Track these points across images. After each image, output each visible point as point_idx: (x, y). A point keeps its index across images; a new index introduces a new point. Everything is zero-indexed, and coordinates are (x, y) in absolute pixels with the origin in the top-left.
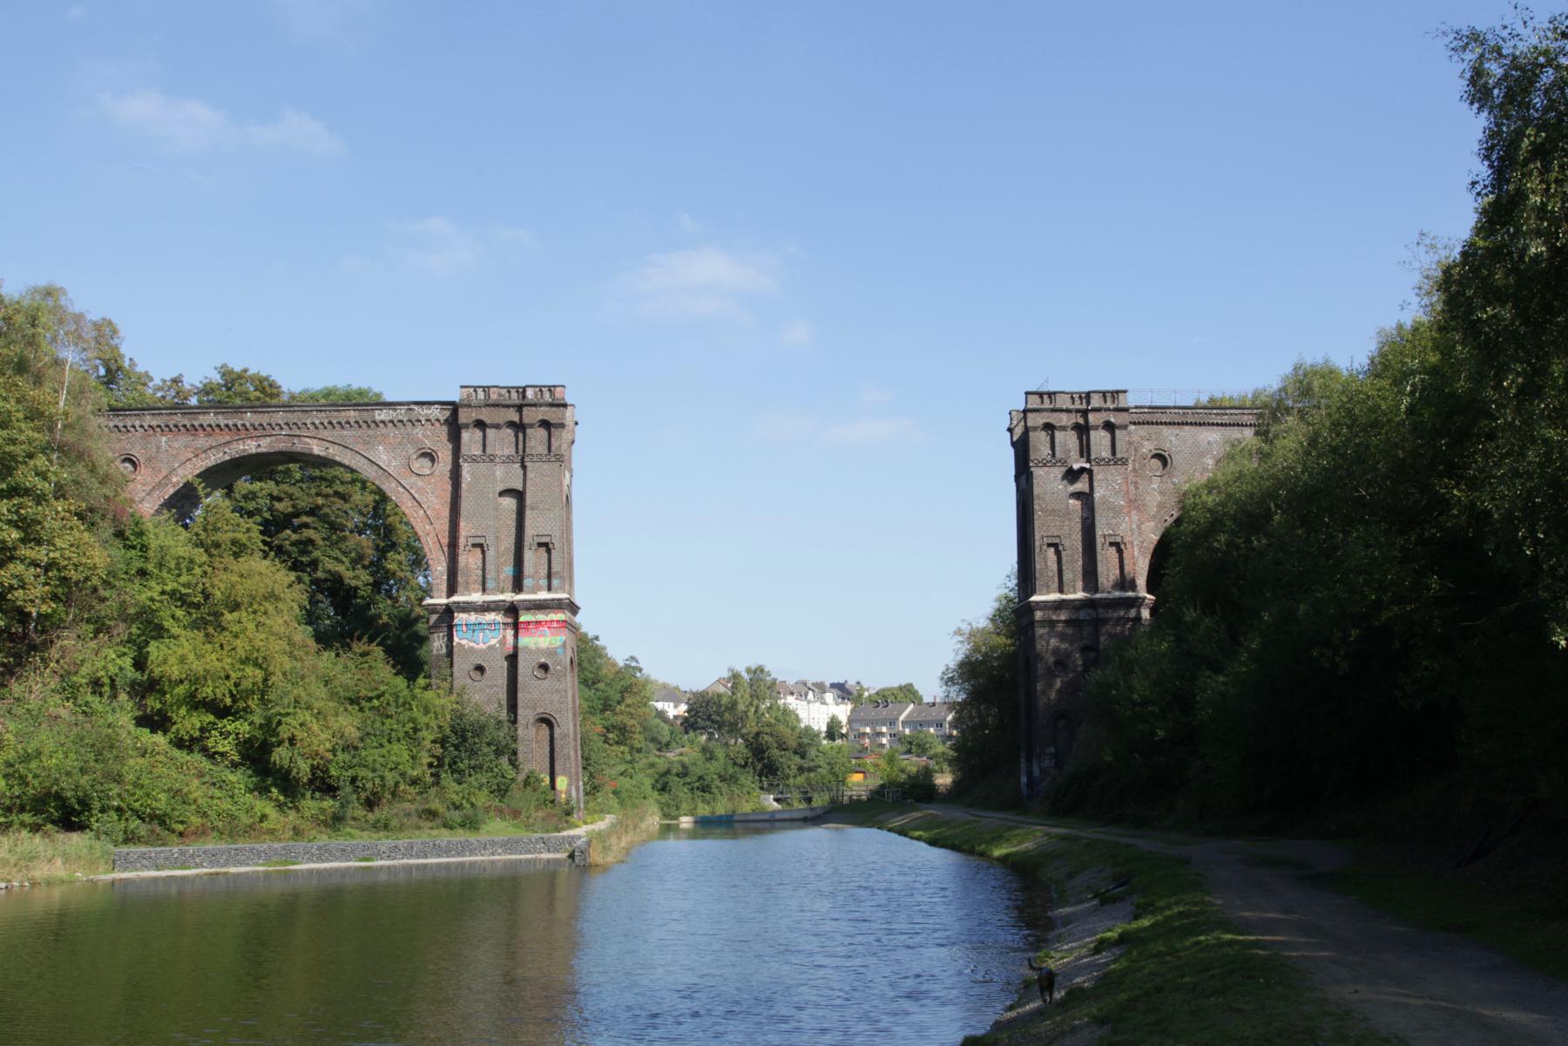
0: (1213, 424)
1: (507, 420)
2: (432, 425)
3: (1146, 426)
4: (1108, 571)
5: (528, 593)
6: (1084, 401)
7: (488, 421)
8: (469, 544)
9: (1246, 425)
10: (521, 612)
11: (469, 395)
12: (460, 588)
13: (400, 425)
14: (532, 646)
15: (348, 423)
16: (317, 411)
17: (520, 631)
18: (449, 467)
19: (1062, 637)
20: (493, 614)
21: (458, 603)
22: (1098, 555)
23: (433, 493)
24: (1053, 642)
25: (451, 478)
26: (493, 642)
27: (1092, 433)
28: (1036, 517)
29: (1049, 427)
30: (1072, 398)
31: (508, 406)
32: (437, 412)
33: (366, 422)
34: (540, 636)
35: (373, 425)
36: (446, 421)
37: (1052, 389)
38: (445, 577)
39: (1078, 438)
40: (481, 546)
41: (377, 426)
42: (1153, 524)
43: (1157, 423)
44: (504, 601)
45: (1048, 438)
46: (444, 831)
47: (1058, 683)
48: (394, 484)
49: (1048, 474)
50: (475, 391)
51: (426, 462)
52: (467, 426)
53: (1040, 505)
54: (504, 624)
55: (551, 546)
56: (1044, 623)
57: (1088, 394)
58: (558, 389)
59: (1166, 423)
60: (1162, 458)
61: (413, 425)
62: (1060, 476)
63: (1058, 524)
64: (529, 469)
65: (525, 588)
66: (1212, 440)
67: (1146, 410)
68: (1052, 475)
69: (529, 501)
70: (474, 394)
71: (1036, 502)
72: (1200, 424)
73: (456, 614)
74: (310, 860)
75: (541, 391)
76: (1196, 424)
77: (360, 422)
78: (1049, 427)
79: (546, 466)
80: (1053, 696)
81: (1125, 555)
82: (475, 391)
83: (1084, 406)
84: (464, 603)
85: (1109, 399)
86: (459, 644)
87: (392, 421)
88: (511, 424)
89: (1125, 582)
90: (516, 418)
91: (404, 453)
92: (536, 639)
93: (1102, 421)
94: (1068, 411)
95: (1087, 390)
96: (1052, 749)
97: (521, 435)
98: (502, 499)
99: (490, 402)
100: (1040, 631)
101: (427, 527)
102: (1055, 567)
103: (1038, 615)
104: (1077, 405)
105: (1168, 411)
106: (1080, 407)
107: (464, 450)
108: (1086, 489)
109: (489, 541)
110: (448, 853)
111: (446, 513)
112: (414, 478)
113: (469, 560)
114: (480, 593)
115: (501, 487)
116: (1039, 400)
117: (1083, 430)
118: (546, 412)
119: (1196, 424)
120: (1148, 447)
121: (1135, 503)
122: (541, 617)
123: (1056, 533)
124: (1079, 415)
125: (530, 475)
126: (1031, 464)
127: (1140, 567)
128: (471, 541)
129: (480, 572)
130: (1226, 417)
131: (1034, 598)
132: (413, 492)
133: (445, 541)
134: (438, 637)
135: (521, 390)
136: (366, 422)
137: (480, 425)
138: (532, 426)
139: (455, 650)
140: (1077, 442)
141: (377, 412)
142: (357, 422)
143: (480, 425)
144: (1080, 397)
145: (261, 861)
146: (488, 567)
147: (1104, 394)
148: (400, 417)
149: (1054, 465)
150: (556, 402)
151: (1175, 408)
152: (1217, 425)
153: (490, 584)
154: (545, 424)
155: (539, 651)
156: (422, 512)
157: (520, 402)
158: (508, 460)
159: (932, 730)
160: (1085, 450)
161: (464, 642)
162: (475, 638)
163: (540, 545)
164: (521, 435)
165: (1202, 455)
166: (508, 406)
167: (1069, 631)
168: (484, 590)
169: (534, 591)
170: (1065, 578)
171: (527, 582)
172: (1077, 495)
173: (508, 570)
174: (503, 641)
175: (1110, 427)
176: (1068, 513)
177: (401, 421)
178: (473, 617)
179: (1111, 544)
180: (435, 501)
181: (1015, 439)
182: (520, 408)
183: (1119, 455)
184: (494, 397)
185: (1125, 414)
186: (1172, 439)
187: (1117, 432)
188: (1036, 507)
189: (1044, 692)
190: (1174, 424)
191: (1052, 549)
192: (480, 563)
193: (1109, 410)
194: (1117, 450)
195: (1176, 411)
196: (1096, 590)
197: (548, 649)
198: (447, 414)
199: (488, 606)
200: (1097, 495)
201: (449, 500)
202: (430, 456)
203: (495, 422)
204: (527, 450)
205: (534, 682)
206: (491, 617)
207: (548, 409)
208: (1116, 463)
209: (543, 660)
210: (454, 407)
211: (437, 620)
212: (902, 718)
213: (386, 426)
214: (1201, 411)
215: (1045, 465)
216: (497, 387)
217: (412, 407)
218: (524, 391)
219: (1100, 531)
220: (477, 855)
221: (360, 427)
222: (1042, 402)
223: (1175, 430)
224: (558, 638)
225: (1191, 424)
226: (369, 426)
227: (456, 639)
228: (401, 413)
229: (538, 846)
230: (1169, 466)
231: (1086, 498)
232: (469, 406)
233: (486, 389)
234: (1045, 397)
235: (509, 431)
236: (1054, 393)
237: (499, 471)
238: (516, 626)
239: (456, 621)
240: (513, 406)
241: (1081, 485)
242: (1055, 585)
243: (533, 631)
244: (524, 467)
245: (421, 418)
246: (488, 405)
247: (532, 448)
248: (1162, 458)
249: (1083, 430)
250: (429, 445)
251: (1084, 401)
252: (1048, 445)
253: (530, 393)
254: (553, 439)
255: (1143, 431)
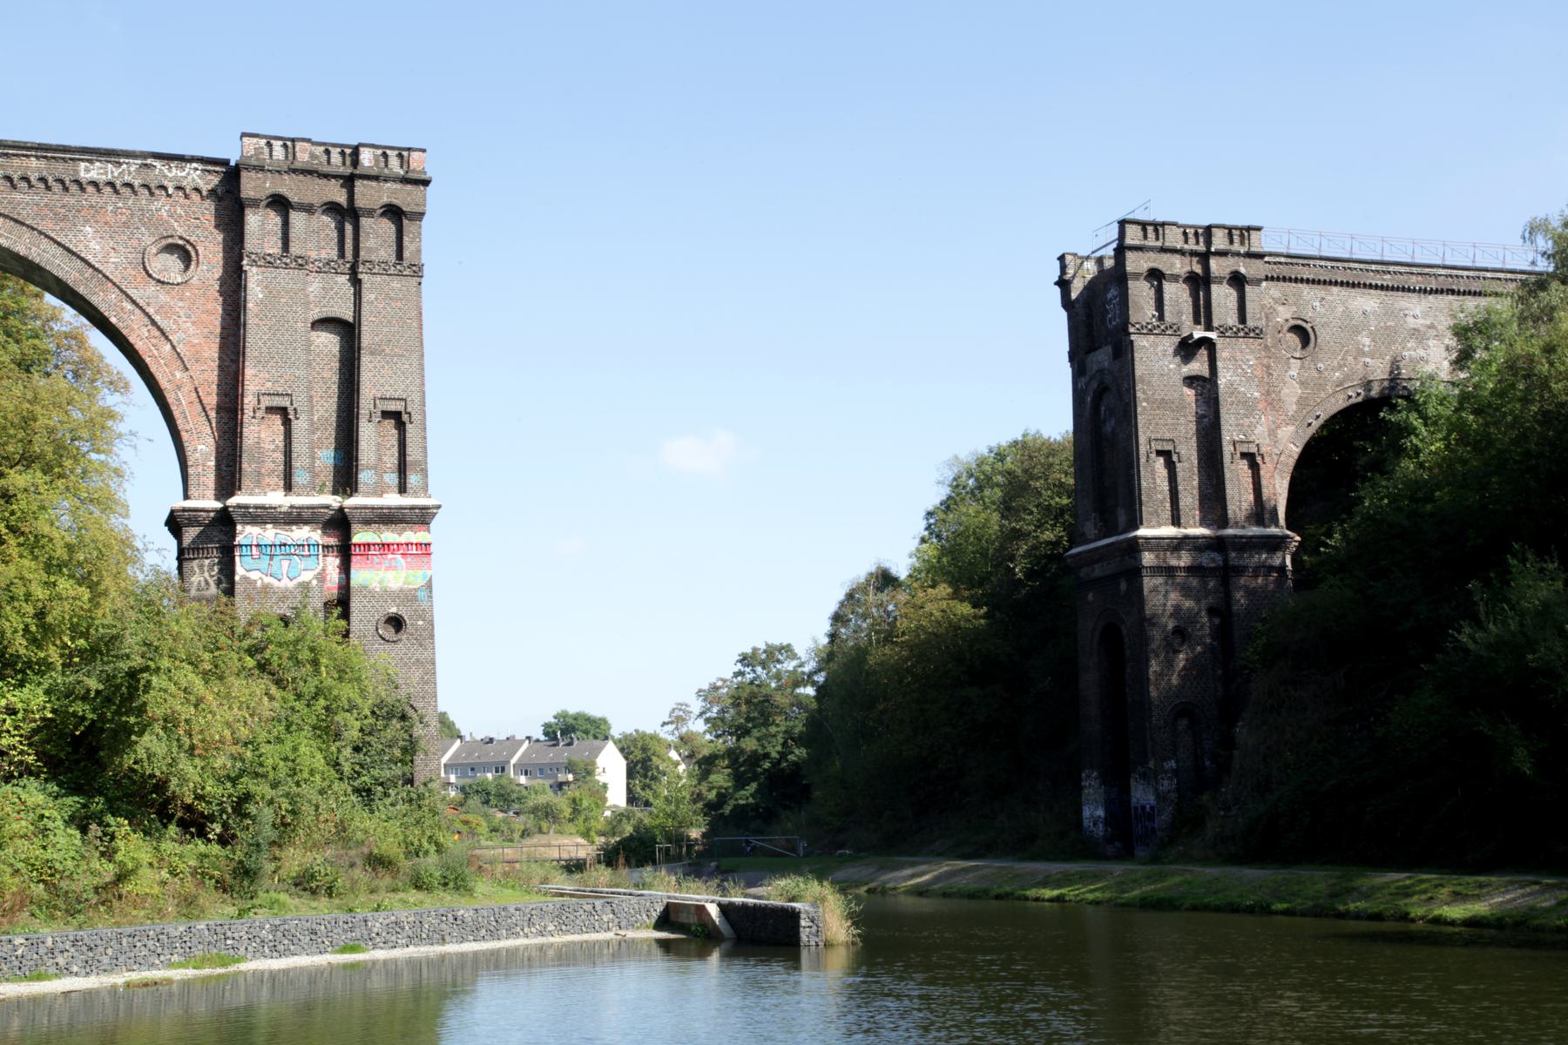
0: (1371, 286)
1: (326, 200)
2: (187, 197)
3: (1281, 284)
4: (1239, 497)
5: (367, 494)
6: (1201, 239)
7: (294, 199)
8: (263, 406)
9: (1414, 291)
10: (355, 527)
11: (258, 150)
12: (246, 482)
13: (126, 191)
14: (375, 585)
15: (25, 179)
16: (37, 157)
17: (354, 559)
18: (218, 272)
19: (1186, 591)
20: (307, 528)
21: (247, 507)
22: (1226, 470)
23: (189, 317)
24: (1174, 597)
25: (221, 293)
26: (307, 576)
27: (1214, 287)
28: (1139, 409)
29: (1156, 276)
30: (1185, 234)
31: (327, 176)
32: (196, 175)
33: (61, 181)
34: (387, 569)
35: (74, 188)
36: (212, 192)
37: (1160, 219)
38: (212, 463)
39: (1191, 295)
40: (283, 411)
41: (83, 189)
42: (1291, 428)
43: (1296, 281)
44: (327, 507)
45: (1152, 292)
46: (413, 896)
47: (1181, 659)
48: (114, 295)
49: (1155, 345)
50: (269, 145)
51: (173, 262)
52: (255, 203)
53: (1144, 393)
54: (323, 546)
55: (405, 417)
56: (1157, 570)
57: (1208, 230)
58: (415, 155)
59: (1308, 281)
60: (1303, 334)
61: (152, 194)
62: (1171, 350)
63: (1170, 421)
64: (365, 286)
65: (361, 487)
66: (1368, 309)
67: (1283, 260)
68: (1160, 348)
69: (367, 339)
70: (266, 150)
71: (1139, 387)
72: (1353, 285)
73: (239, 527)
74: (258, 954)
75: (385, 155)
76: (1348, 284)
77: (50, 179)
78: (1156, 276)
79: (396, 283)
80: (1175, 680)
81: (1262, 473)
82: (269, 145)
83: (1201, 248)
84: (256, 507)
85: (1236, 239)
86: (245, 578)
87: (111, 184)
88: (332, 208)
89: (1261, 512)
90: (341, 198)
91: (135, 243)
92: (381, 574)
93: (1228, 270)
94: (1181, 252)
95: (1207, 223)
96: (1173, 764)
97: (349, 228)
98: (314, 334)
99: (297, 165)
100: (1148, 583)
101: (178, 375)
102: (1164, 486)
103: (1148, 558)
104: (1191, 246)
105: (1312, 262)
106: (1195, 248)
107: (250, 244)
108: (1205, 372)
109: (300, 401)
110: (475, 932)
111: (212, 351)
112: (152, 288)
113: (260, 434)
114: (281, 493)
115: (316, 314)
116: (1140, 234)
117: (1199, 283)
118: (395, 192)
119: (1348, 284)
120: (1284, 315)
121: (1272, 400)
122: (389, 536)
123: (1168, 436)
124: (1195, 259)
125: (367, 296)
126: (1132, 330)
127: (1278, 489)
128: (266, 402)
129: (280, 457)
130: (1388, 276)
131: (1142, 532)
132: (151, 311)
133: (212, 400)
134: (201, 567)
135: (348, 151)
136: (61, 181)
137: (280, 204)
138: (370, 213)
139: (238, 589)
140: (1190, 300)
141: (83, 165)
142: (43, 180)
143: (280, 204)
144: (1196, 234)
145: (175, 958)
146: (299, 447)
147: (1230, 230)
148: (127, 178)
149: (1163, 333)
150: (410, 175)
151: (1321, 258)
152: (1377, 287)
153: (300, 477)
154: (394, 213)
155: (387, 594)
156: (168, 347)
157: (348, 171)
158: (327, 267)
159: (489, 776)
160: (1203, 313)
161: (254, 576)
162: (274, 569)
163: (386, 415)
164: (349, 228)
165: (1356, 331)
166: (327, 176)
167: (1194, 582)
168: (288, 487)
169: (380, 491)
170: (1182, 504)
171: (365, 477)
172: (1191, 381)
173: (326, 457)
174: (321, 577)
175: (1237, 281)
176: (1182, 407)
177: (128, 185)
178: (270, 534)
179: (1244, 455)
180: (191, 331)
181: (1074, 296)
182: (349, 181)
183: (1250, 323)
184: (303, 155)
185: (1258, 262)
186: (1316, 304)
187: (1248, 288)
188: (1139, 394)
189: (1160, 675)
190: (1319, 282)
191: (1161, 460)
192: (280, 440)
193: (1238, 254)
194: (1249, 316)
195: (1323, 263)
196: (1223, 521)
197: (401, 590)
198: (215, 180)
199: (299, 514)
200: (1222, 381)
201: (218, 330)
202: (184, 253)
203: (306, 201)
204: (362, 253)
205: (379, 646)
206: (302, 533)
207: (398, 186)
208: (1246, 336)
209: (394, 610)
210: (232, 175)
211: (198, 536)
212: (513, 761)
213: (99, 190)
214: (1356, 265)
215: (1150, 332)
216: (309, 141)
217: (149, 161)
218: (356, 151)
219: (1229, 433)
220: (517, 935)
221: (48, 188)
222: (1145, 237)
223: (1319, 291)
224: (420, 573)
225: (1342, 284)
226: (66, 189)
227: (240, 571)
228: (129, 171)
229: (605, 918)
230: (1312, 344)
231: (1206, 387)
232: (261, 169)
233: (290, 143)
234: (1150, 229)
235: (326, 219)
236: (1163, 224)
237: (315, 285)
238: (345, 552)
239: (239, 539)
240: (335, 177)
241: (1199, 366)
242: (1167, 514)
243: (376, 559)
244: (356, 282)
245: (166, 183)
246: (294, 171)
247: (370, 250)
248: (1303, 334)
249: (1199, 283)
250: (180, 231)
251: (1201, 239)
252: (1152, 302)
253: (366, 157)
254: (406, 239)
255: (1273, 290)
